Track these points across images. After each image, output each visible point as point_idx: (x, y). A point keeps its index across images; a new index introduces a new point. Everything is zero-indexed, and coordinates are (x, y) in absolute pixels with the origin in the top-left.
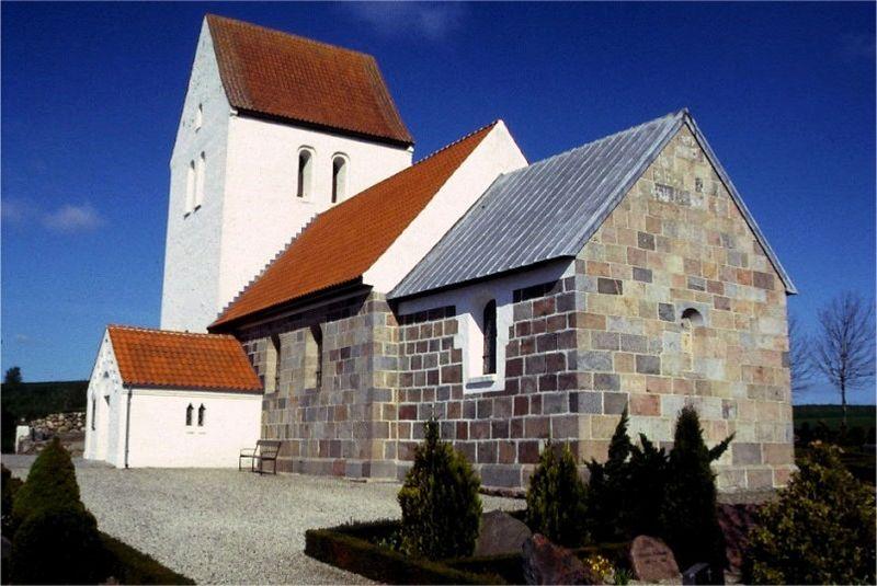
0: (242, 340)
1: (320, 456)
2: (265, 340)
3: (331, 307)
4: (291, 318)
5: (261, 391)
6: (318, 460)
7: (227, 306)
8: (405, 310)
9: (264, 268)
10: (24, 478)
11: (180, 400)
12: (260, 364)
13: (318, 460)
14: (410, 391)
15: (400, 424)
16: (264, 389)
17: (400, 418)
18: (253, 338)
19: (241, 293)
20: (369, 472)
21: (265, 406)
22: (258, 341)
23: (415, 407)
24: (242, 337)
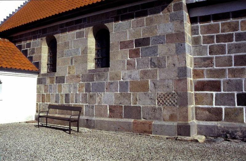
0: (15, 42)
1: (110, 117)
2: (39, 40)
3: (119, 12)
4: (67, 24)
5: (38, 73)
6: (107, 119)
7: (8, 16)
8: (199, 13)
9: (17, 9)
10: (174, 45)
11: (74, 32)
12: (34, 55)
13: (107, 119)
14: (229, 69)
15: (196, 95)
16: (40, 70)
17: (195, 90)
18: (27, 40)
19: (5, 19)
20: (178, 129)
21: (39, 82)
22: (32, 41)
23: (220, 82)
24: (14, 40)
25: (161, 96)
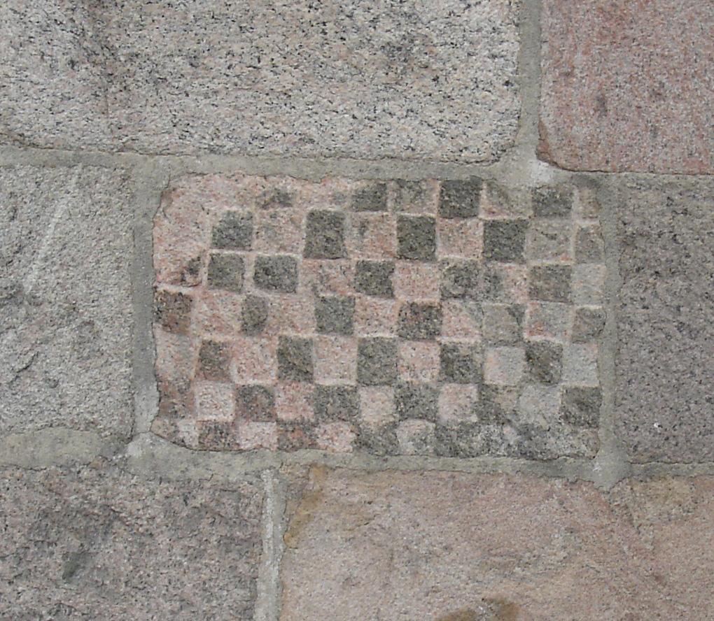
25: (260, 250)
